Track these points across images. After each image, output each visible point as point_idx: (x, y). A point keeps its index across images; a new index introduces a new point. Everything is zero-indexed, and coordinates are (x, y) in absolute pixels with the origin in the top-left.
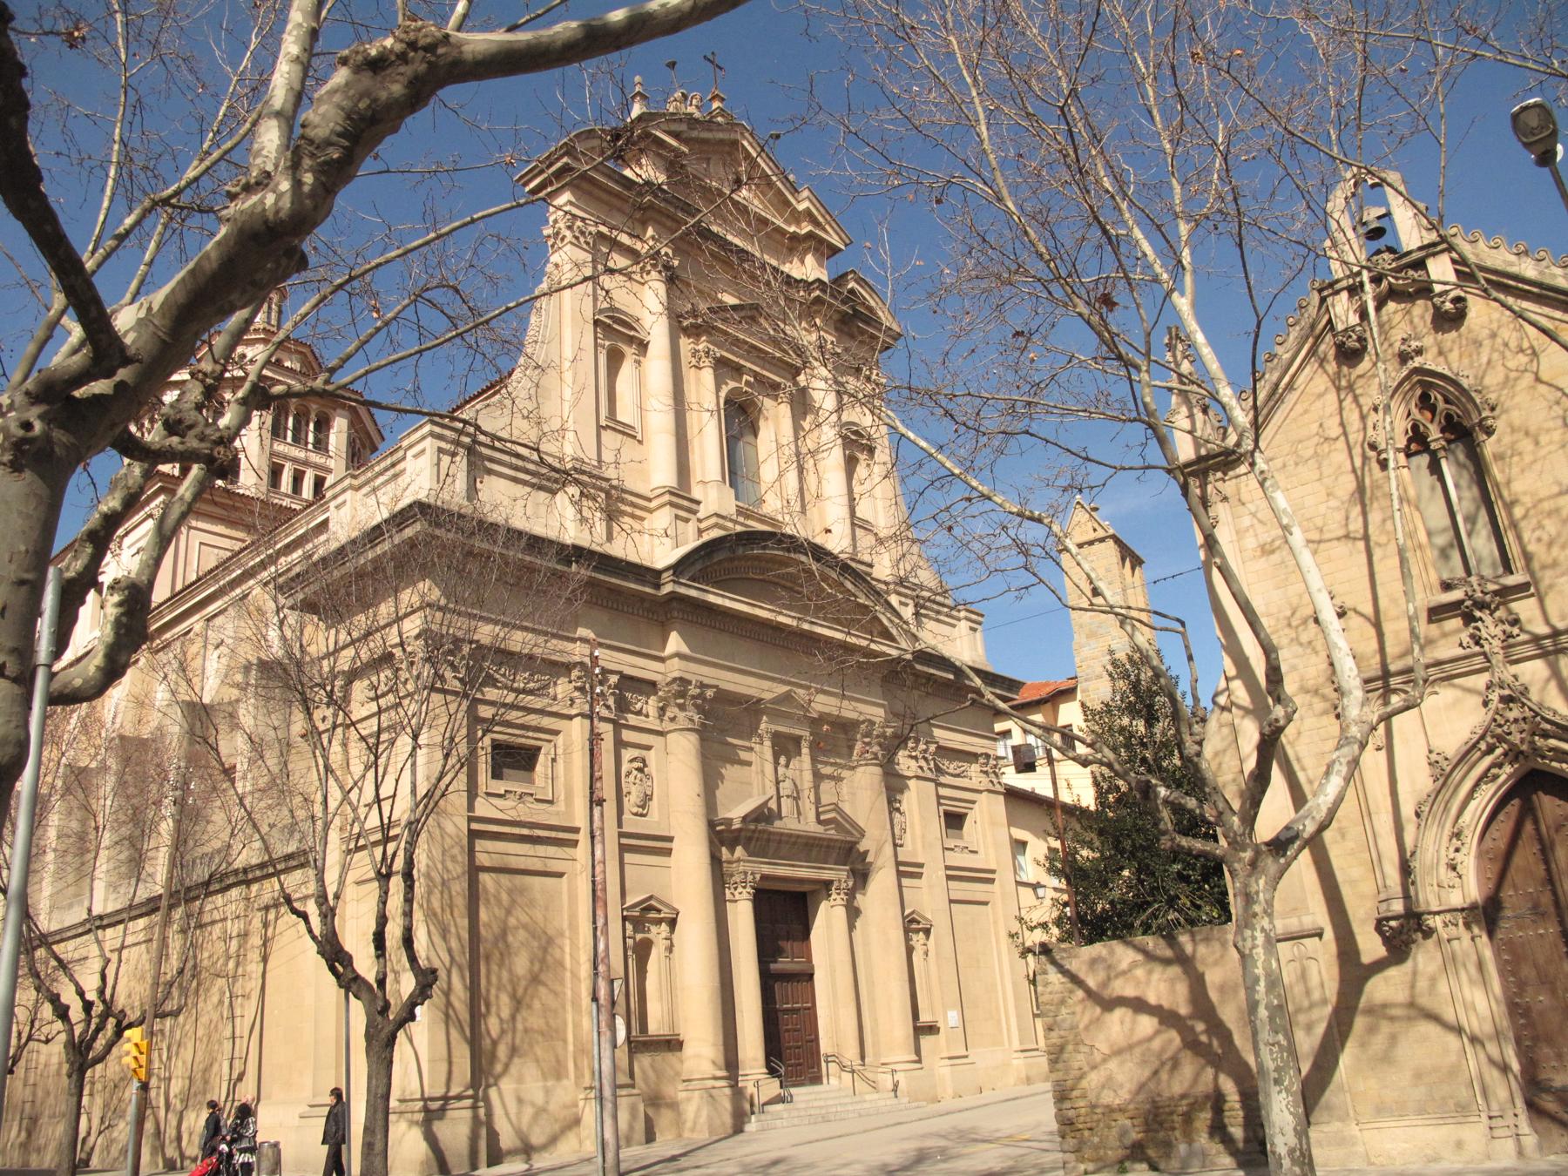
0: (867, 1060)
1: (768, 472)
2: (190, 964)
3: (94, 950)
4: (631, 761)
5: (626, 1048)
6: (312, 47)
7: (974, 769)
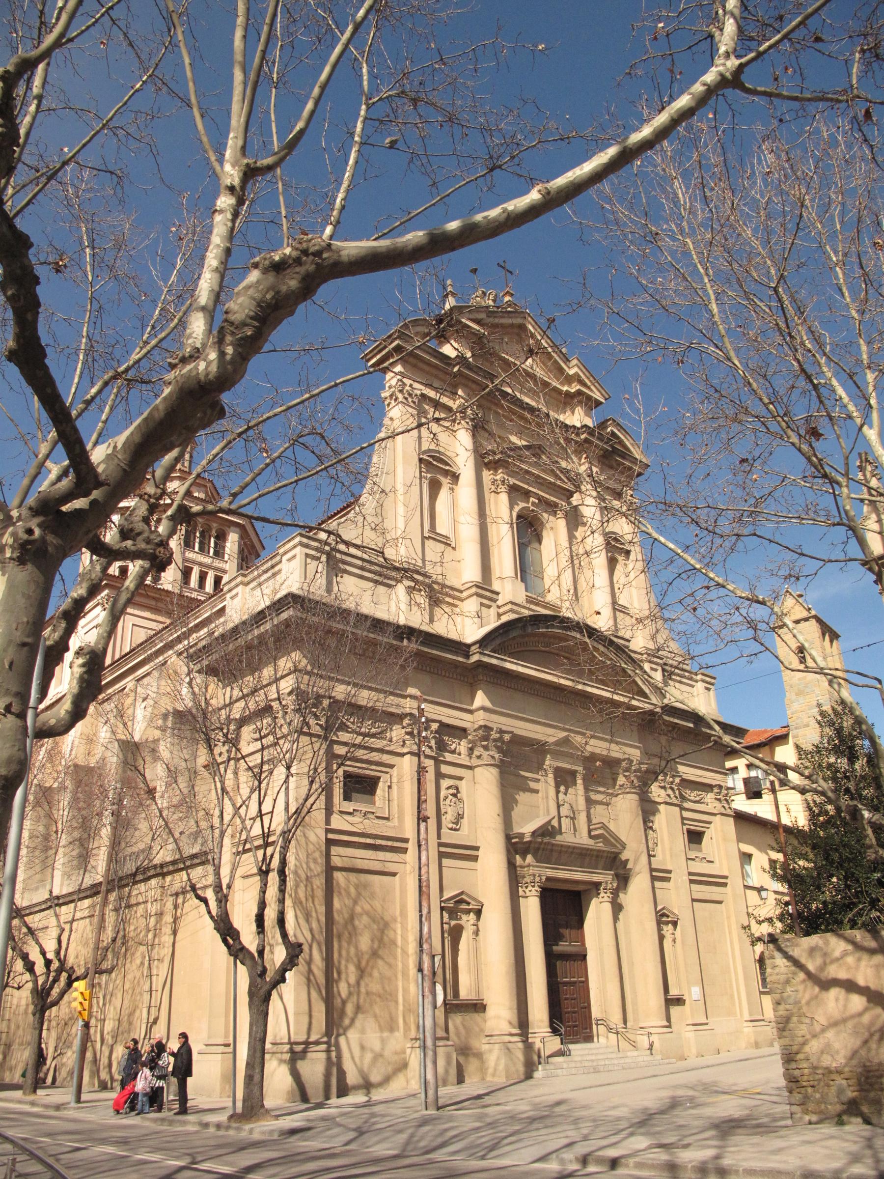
0: (629, 1024)
1: (550, 571)
2: (121, 933)
3: (53, 921)
4: (448, 788)
5: (443, 1009)
6: (226, 260)
7: (710, 797)
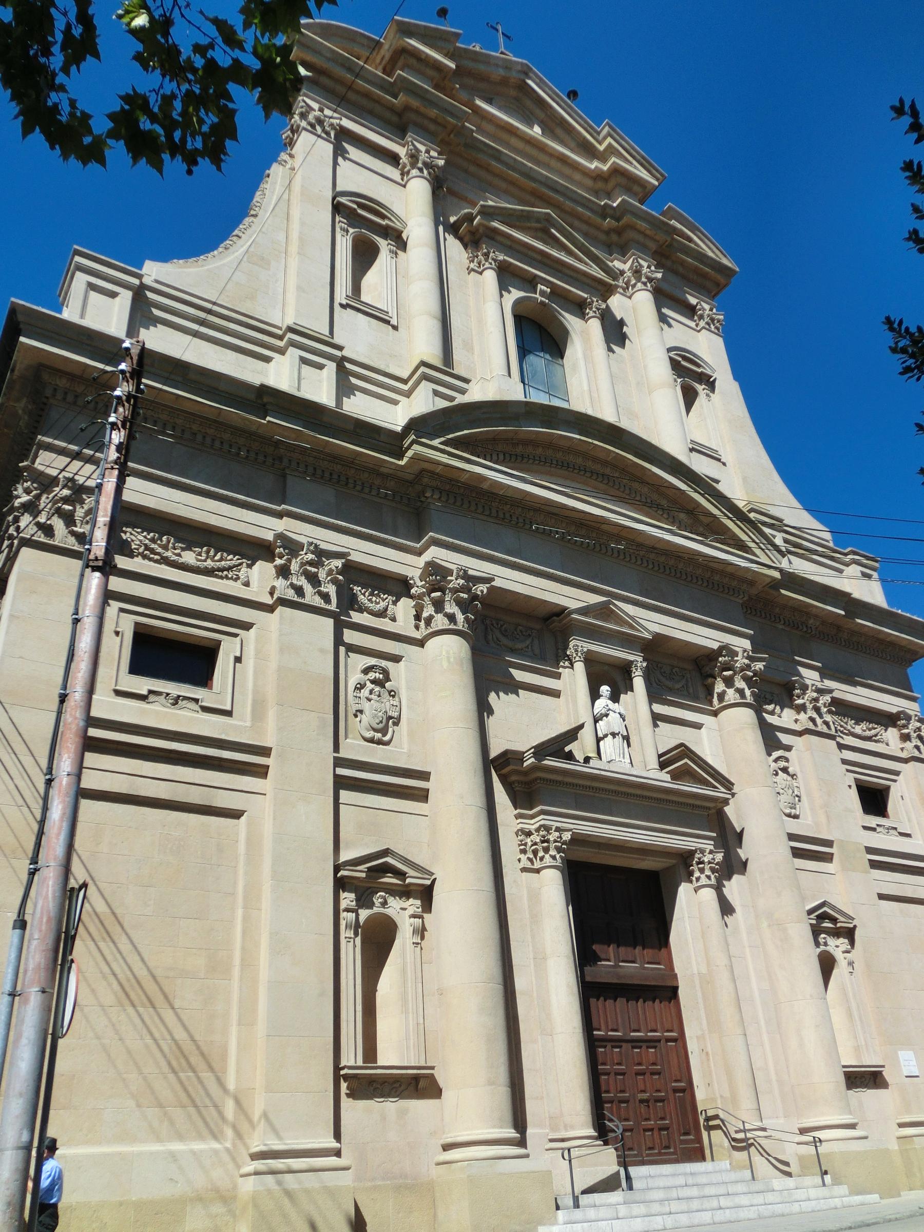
4: (366, 671)
7: (891, 734)
